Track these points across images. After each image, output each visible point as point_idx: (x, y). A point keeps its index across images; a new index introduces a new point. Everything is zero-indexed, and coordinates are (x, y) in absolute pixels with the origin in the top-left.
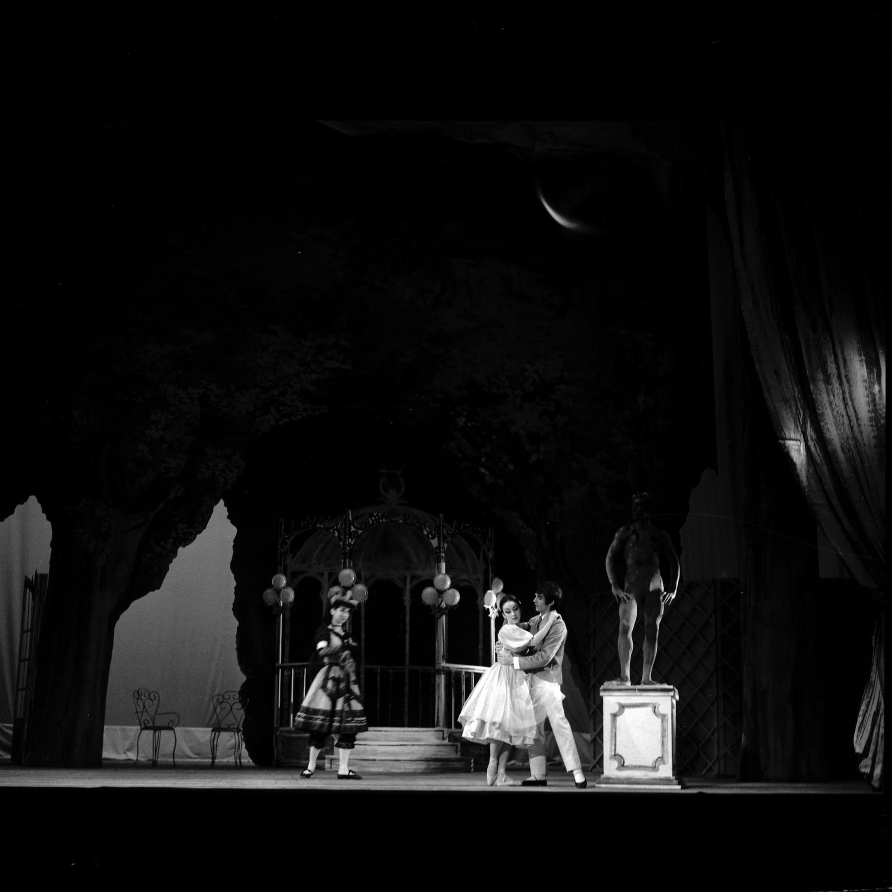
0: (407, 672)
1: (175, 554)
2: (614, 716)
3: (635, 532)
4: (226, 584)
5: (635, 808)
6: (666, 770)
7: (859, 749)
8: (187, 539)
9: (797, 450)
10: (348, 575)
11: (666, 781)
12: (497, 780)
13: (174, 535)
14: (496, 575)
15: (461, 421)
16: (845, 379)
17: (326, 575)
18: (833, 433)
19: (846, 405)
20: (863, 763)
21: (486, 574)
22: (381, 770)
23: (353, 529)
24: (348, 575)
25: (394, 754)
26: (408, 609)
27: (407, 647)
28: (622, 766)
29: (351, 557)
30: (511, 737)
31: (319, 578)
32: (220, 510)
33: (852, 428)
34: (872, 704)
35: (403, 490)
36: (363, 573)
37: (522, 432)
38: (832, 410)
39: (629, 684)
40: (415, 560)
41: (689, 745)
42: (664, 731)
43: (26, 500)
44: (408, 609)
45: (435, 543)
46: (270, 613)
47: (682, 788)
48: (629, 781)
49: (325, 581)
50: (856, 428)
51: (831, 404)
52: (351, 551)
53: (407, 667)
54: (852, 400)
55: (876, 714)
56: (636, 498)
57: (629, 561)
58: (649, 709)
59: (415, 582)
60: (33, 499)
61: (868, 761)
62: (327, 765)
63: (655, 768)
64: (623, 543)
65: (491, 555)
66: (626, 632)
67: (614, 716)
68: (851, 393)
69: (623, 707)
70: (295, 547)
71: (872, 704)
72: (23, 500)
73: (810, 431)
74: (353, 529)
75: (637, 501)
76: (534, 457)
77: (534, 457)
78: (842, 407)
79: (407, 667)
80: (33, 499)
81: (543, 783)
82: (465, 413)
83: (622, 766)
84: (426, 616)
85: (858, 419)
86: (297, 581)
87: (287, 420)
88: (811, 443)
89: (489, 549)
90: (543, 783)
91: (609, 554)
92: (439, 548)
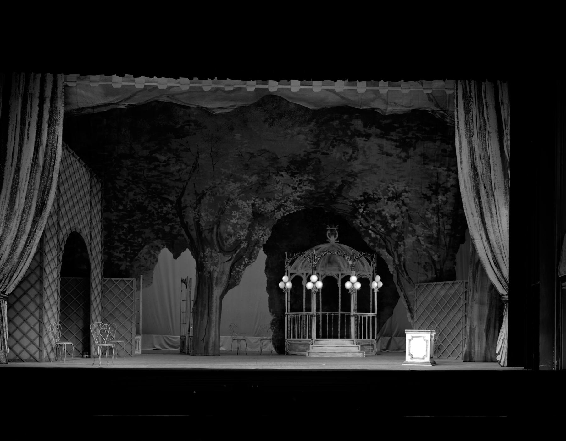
0: (340, 315)
2: (410, 340)
4: (264, 278)
6: (427, 359)
7: (497, 352)
10: (314, 278)
11: (427, 363)
13: (244, 263)
15: (361, 211)
17: (305, 274)
22: (328, 356)
23: (316, 258)
25: (333, 350)
26: (340, 289)
27: (340, 304)
28: (412, 358)
31: (302, 276)
35: (337, 236)
37: (387, 214)
40: (342, 266)
41: (437, 350)
42: (427, 346)
43: (185, 250)
44: (340, 289)
46: (281, 292)
48: (414, 363)
49: (305, 278)
51: (492, 225)
53: (340, 313)
58: (422, 338)
60: (187, 250)
62: (307, 355)
63: (423, 359)
67: (410, 340)
69: (413, 337)
70: (291, 264)
74: (316, 258)
77: (392, 225)
79: (340, 313)
80: (187, 250)
82: (363, 207)
83: (412, 358)
84: (346, 293)
86: (293, 277)
87: (288, 213)
88: (485, 243)
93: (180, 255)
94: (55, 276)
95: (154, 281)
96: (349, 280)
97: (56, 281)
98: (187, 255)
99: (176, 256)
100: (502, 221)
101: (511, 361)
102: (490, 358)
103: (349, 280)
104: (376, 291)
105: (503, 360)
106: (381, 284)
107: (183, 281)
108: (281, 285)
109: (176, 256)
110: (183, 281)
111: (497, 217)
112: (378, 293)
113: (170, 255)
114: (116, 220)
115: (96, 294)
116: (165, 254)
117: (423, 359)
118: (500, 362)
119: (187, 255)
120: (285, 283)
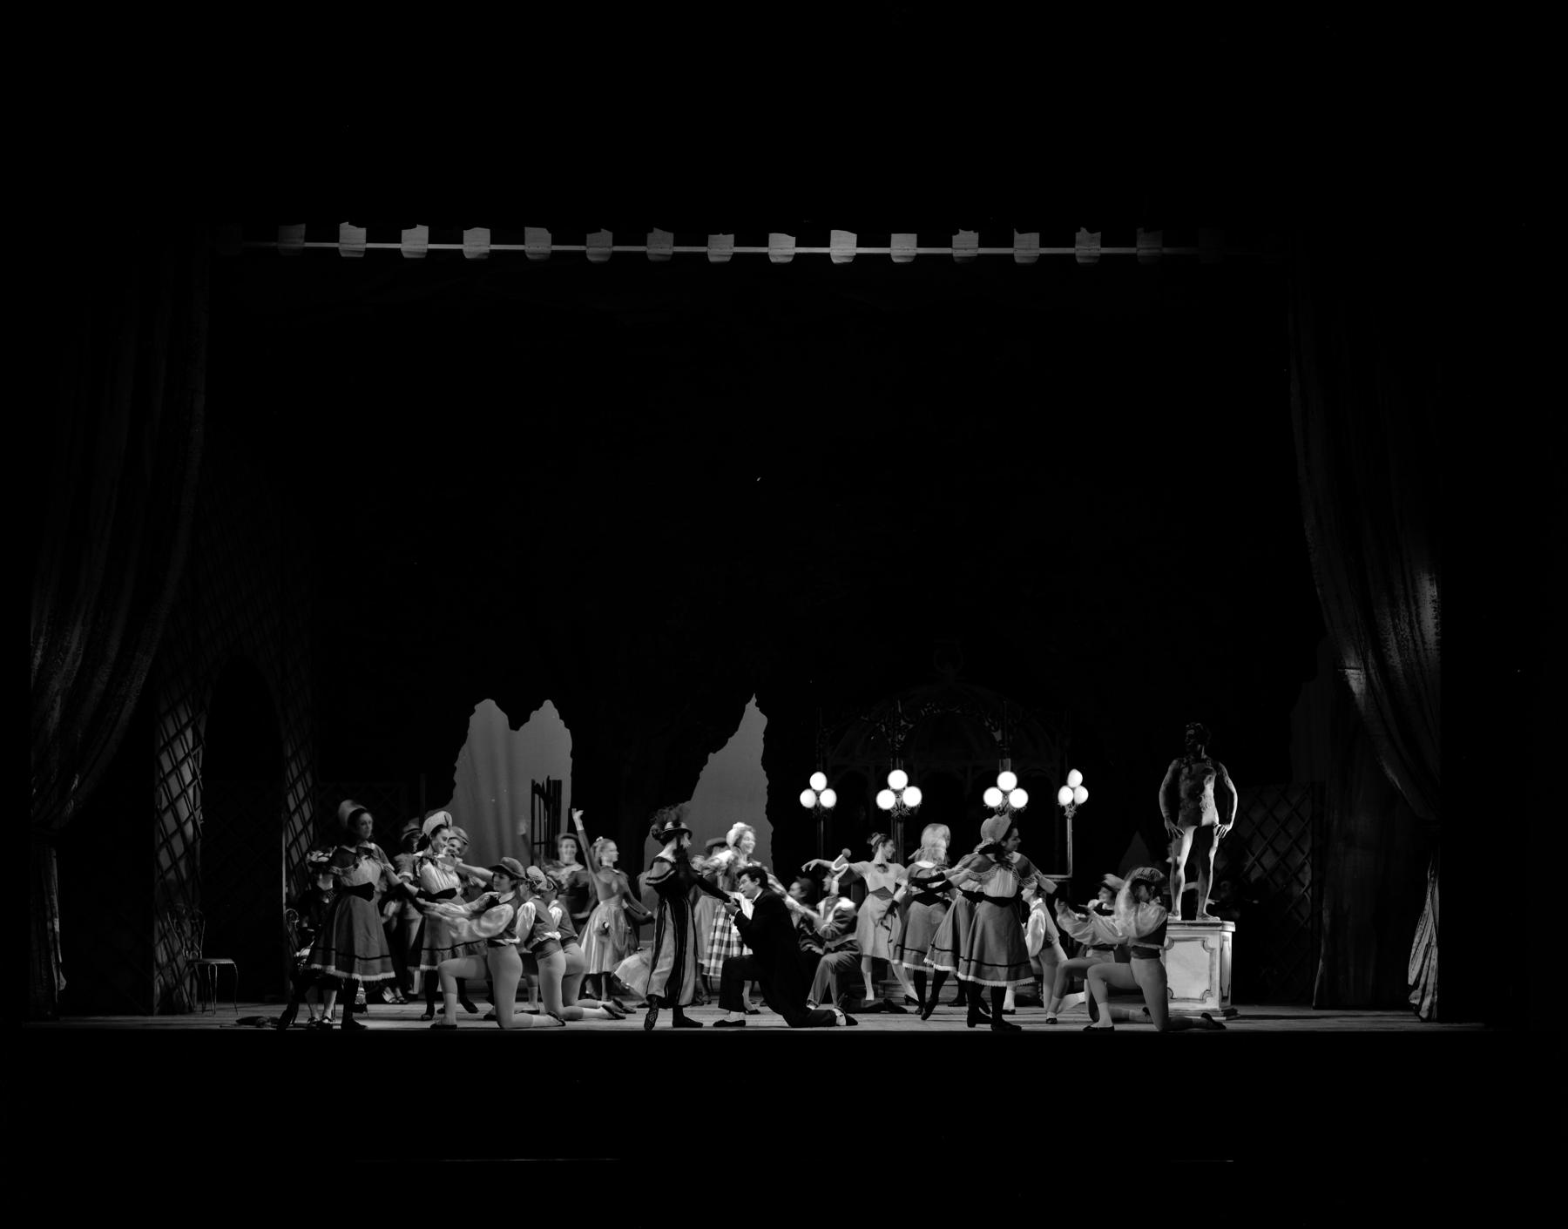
1: (705, 762)
3: (1188, 765)
4: (760, 781)
5: (1185, 1039)
7: (1411, 981)
8: (719, 744)
9: (1356, 679)
16: (1413, 600)
18: (1396, 660)
19: (1412, 628)
20: (1413, 994)
30: (969, 995)
33: (1417, 652)
34: (1426, 935)
38: (1396, 634)
39: (1179, 918)
41: (1248, 979)
45: (998, 736)
50: (1422, 654)
51: (1395, 627)
54: (1419, 623)
55: (1429, 945)
56: (1196, 728)
57: (1183, 795)
58: (1199, 943)
60: (548, 704)
61: (1418, 993)
64: (1177, 773)
66: (1177, 867)
68: (1418, 615)
71: (1426, 935)
72: (538, 706)
73: (1371, 660)
75: (1191, 732)
80: (548, 704)
81: (1013, 1012)
85: (1424, 643)
88: (1372, 671)
90: (1013, 1012)
91: (1163, 788)
93: (527, 720)
94: (188, 778)
95: (457, 791)
96: (995, 785)
97: (191, 792)
98: (547, 716)
99: (517, 720)
100: (1423, 616)
101: (1443, 1009)
102: (1395, 995)
103: (995, 785)
104: (1069, 814)
105: (1427, 1002)
106: (1083, 795)
107: (536, 789)
108: (807, 799)
109: (517, 720)
110: (536, 789)
111: (1408, 606)
112: (1074, 819)
113: (501, 718)
114: (968, 878)
115: (299, 827)
116: (488, 715)
117: (1202, 1000)
118: (1419, 1007)
119: (547, 716)
120: (818, 794)
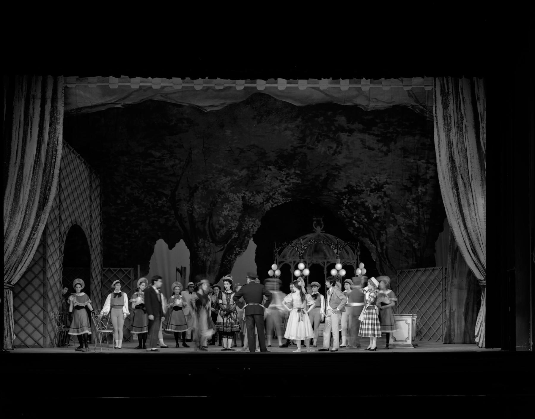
6: (410, 342)
7: (476, 334)
10: (301, 266)
12: (299, 350)
13: (235, 252)
14: (361, 261)
15: (345, 202)
17: (293, 263)
21: (357, 260)
23: (303, 247)
24: (301, 266)
28: (395, 340)
29: (302, 258)
31: (290, 264)
32: (251, 241)
35: (323, 226)
36: (307, 261)
37: (370, 205)
40: (328, 255)
42: (409, 329)
45: (335, 251)
47: (261, 351)
49: (293, 266)
52: (303, 256)
58: (404, 322)
59: (329, 264)
60: (182, 241)
65: (359, 253)
70: (280, 253)
72: (178, 241)
74: (303, 247)
76: (375, 216)
77: (375, 216)
78: (474, 215)
83: (395, 340)
86: (281, 265)
89: (358, 251)
92: (337, 253)
